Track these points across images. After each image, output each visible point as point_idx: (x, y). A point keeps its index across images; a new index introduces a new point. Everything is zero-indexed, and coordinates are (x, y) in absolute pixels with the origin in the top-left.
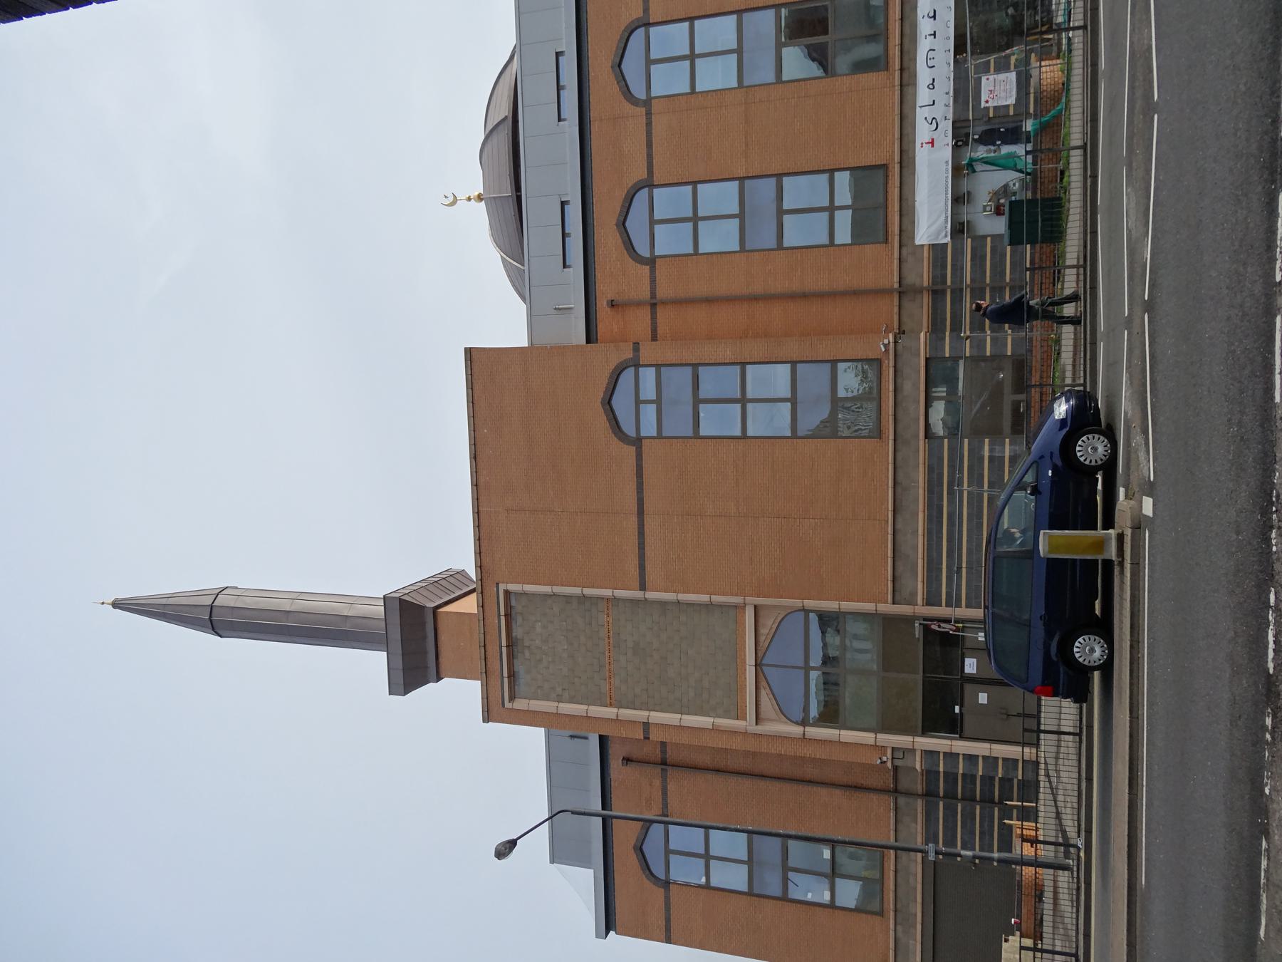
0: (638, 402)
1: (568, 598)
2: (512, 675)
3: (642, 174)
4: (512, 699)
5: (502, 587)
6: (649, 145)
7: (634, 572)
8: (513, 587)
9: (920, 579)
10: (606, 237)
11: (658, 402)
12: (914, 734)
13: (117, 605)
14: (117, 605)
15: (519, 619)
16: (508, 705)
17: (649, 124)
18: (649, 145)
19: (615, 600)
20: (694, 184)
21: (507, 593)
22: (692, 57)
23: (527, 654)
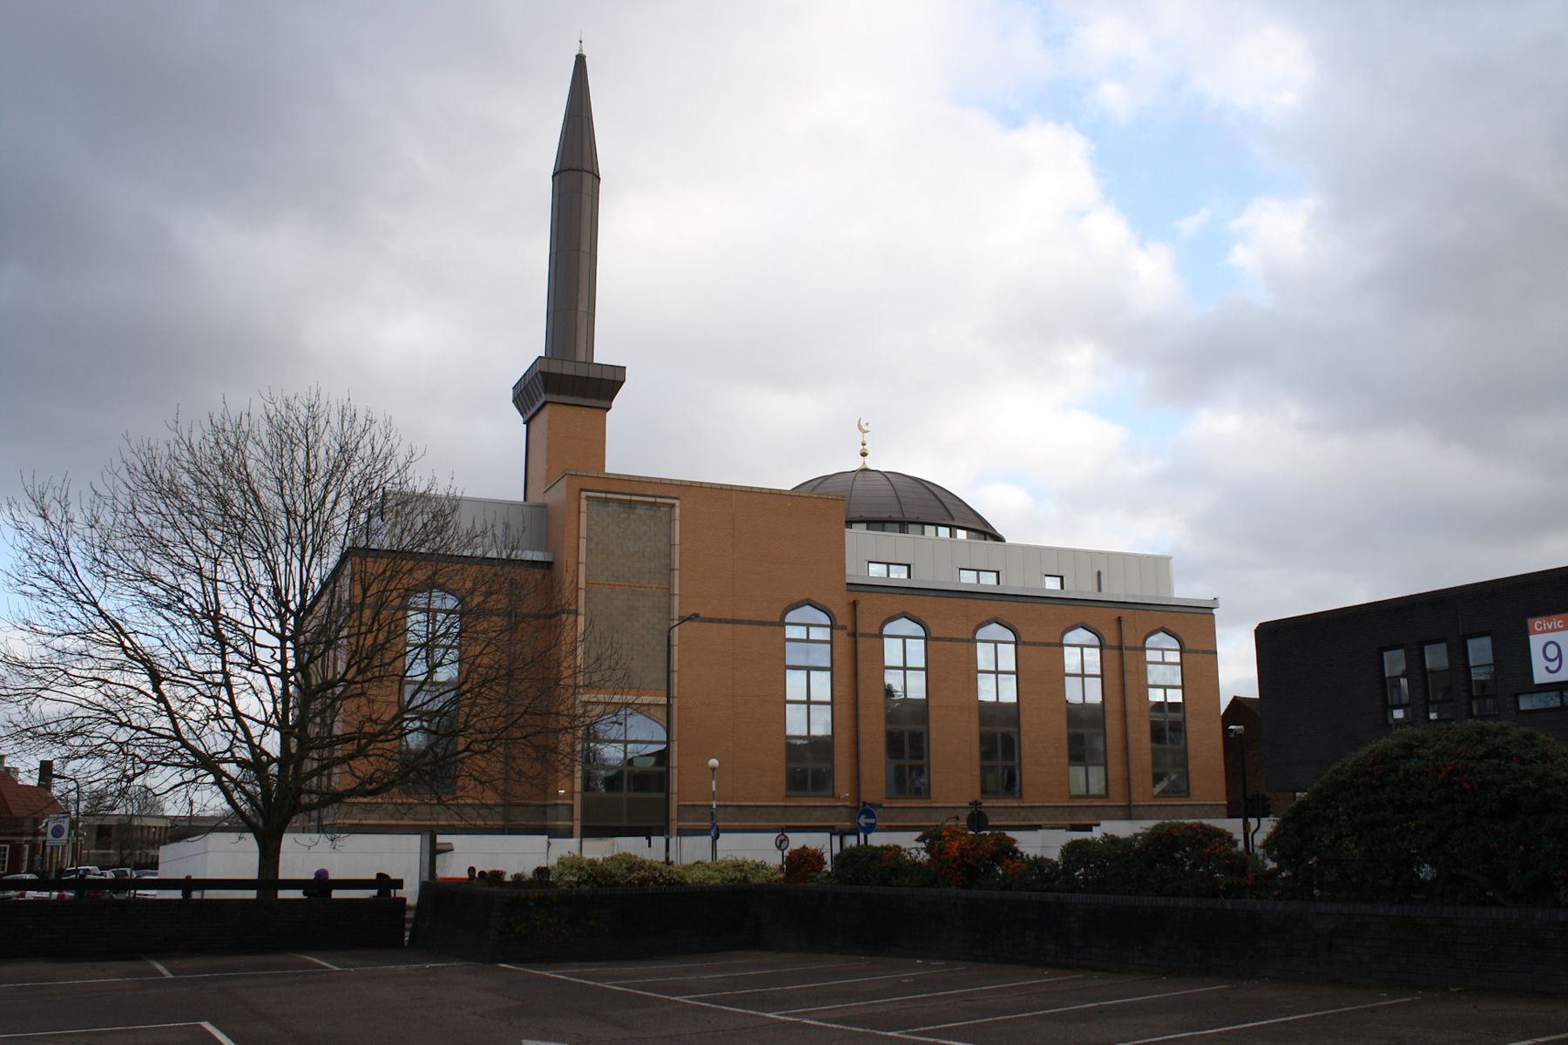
0: (808, 626)
1: (669, 556)
2: (606, 500)
3: (934, 634)
4: (588, 498)
5: (677, 502)
6: (951, 640)
7: (959, 646)
8: (677, 510)
9: (598, 850)
10: (900, 603)
11: (808, 640)
12: (583, 820)
13: (580, 61)
14: (580, 61)
15: (650, 513)
16: (584, 494)
17: (963, 640)
18: (951, 640)
19: (671, 595)
20: (831, 669)
21: (673, 506)
22: (905, 668)
23: (624, 516)
